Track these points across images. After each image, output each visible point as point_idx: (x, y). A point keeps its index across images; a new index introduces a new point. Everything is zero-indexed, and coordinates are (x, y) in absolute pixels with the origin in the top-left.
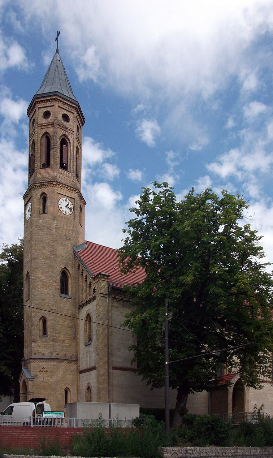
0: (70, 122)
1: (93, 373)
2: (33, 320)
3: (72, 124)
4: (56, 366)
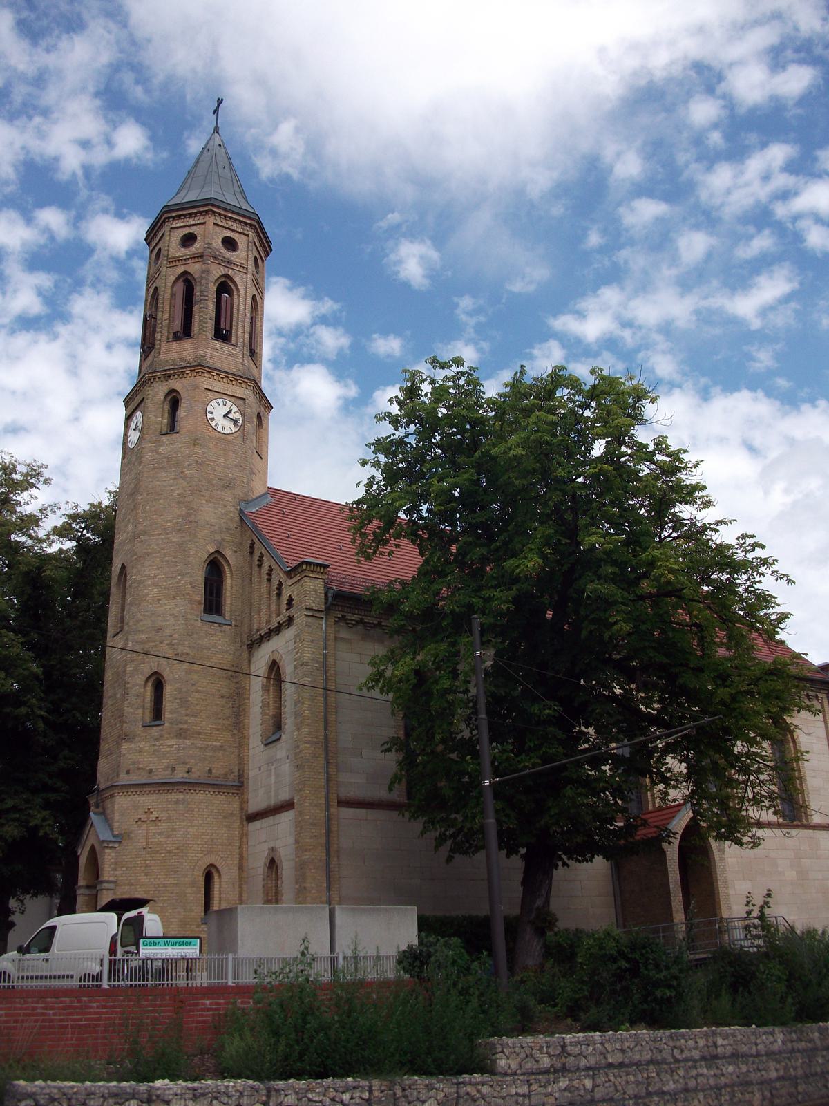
1: (286, 818)
3: (243, 254)
4: (183, 803)
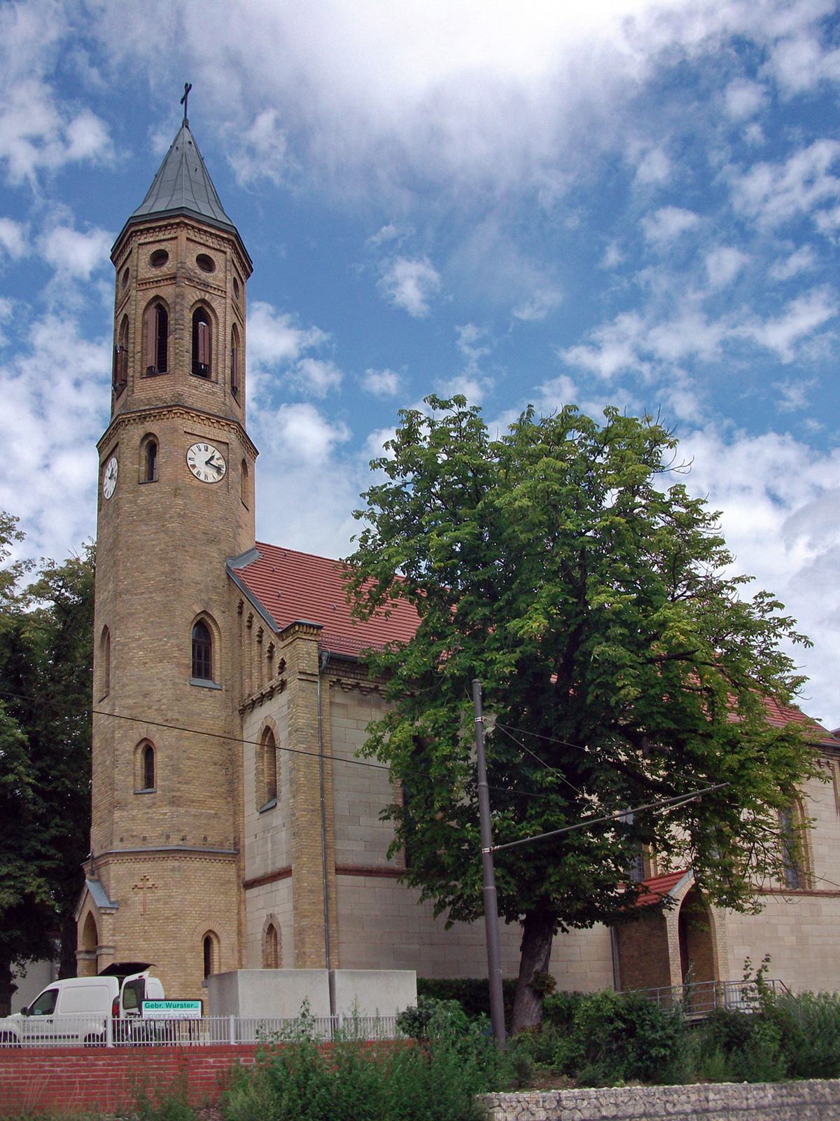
0: (216, 272)
2: (117, 750)
3: (221, 275)
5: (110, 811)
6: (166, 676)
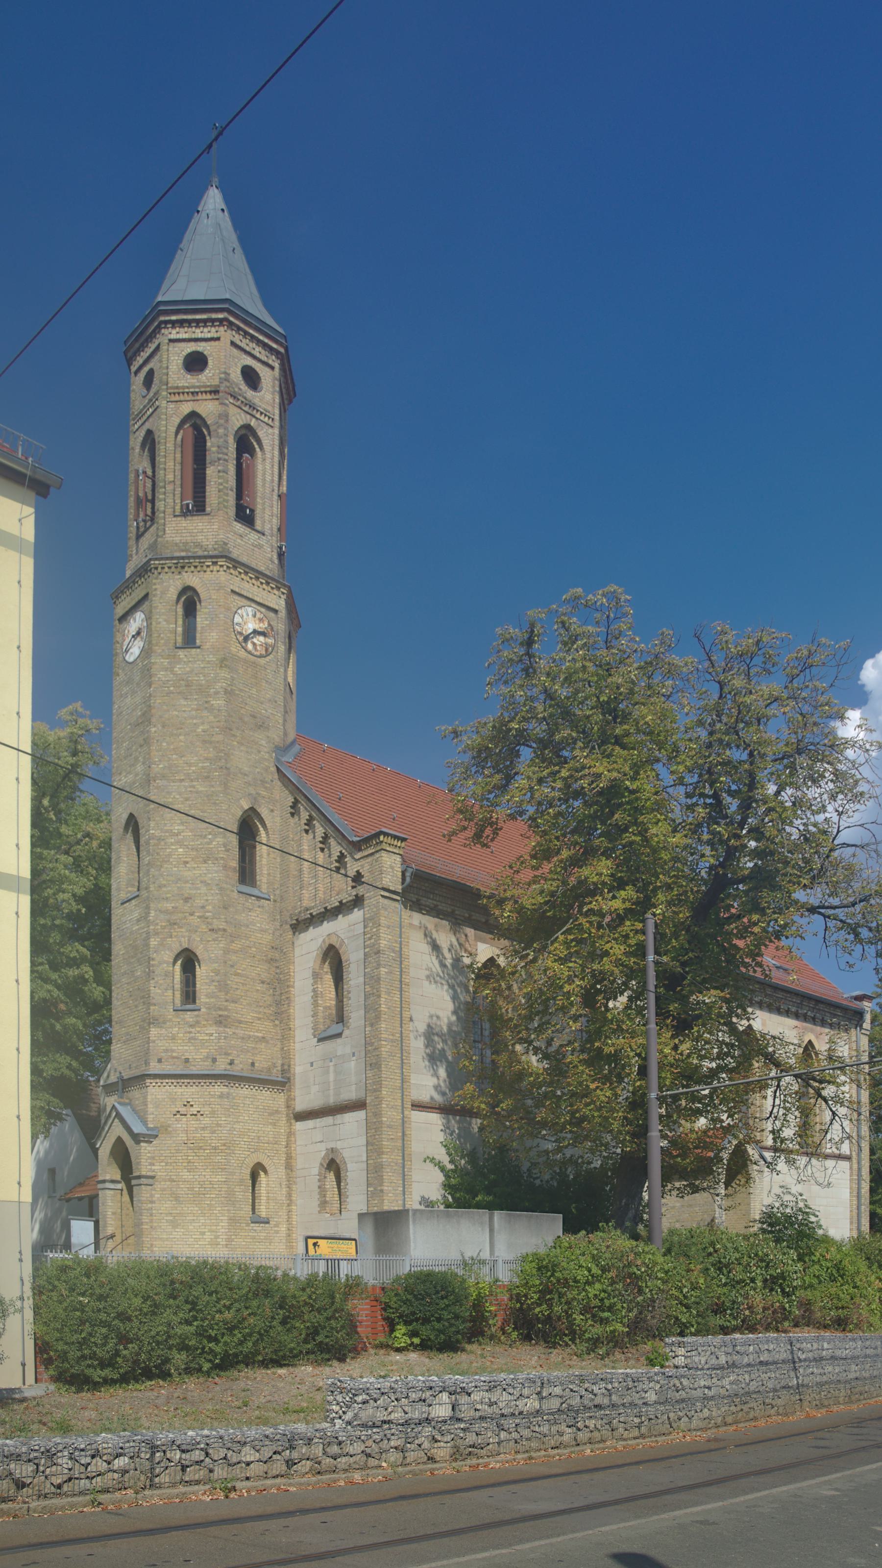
0: (263, 392)
2: (153, 959)
4: (228, 1098)
5: (142, 1028)
6: (211, 879)
